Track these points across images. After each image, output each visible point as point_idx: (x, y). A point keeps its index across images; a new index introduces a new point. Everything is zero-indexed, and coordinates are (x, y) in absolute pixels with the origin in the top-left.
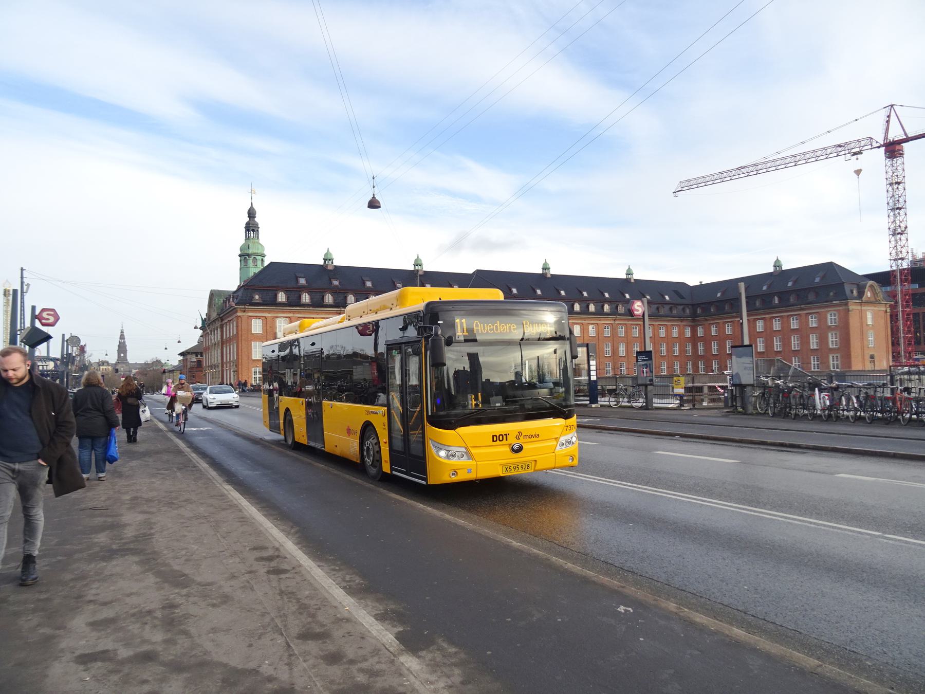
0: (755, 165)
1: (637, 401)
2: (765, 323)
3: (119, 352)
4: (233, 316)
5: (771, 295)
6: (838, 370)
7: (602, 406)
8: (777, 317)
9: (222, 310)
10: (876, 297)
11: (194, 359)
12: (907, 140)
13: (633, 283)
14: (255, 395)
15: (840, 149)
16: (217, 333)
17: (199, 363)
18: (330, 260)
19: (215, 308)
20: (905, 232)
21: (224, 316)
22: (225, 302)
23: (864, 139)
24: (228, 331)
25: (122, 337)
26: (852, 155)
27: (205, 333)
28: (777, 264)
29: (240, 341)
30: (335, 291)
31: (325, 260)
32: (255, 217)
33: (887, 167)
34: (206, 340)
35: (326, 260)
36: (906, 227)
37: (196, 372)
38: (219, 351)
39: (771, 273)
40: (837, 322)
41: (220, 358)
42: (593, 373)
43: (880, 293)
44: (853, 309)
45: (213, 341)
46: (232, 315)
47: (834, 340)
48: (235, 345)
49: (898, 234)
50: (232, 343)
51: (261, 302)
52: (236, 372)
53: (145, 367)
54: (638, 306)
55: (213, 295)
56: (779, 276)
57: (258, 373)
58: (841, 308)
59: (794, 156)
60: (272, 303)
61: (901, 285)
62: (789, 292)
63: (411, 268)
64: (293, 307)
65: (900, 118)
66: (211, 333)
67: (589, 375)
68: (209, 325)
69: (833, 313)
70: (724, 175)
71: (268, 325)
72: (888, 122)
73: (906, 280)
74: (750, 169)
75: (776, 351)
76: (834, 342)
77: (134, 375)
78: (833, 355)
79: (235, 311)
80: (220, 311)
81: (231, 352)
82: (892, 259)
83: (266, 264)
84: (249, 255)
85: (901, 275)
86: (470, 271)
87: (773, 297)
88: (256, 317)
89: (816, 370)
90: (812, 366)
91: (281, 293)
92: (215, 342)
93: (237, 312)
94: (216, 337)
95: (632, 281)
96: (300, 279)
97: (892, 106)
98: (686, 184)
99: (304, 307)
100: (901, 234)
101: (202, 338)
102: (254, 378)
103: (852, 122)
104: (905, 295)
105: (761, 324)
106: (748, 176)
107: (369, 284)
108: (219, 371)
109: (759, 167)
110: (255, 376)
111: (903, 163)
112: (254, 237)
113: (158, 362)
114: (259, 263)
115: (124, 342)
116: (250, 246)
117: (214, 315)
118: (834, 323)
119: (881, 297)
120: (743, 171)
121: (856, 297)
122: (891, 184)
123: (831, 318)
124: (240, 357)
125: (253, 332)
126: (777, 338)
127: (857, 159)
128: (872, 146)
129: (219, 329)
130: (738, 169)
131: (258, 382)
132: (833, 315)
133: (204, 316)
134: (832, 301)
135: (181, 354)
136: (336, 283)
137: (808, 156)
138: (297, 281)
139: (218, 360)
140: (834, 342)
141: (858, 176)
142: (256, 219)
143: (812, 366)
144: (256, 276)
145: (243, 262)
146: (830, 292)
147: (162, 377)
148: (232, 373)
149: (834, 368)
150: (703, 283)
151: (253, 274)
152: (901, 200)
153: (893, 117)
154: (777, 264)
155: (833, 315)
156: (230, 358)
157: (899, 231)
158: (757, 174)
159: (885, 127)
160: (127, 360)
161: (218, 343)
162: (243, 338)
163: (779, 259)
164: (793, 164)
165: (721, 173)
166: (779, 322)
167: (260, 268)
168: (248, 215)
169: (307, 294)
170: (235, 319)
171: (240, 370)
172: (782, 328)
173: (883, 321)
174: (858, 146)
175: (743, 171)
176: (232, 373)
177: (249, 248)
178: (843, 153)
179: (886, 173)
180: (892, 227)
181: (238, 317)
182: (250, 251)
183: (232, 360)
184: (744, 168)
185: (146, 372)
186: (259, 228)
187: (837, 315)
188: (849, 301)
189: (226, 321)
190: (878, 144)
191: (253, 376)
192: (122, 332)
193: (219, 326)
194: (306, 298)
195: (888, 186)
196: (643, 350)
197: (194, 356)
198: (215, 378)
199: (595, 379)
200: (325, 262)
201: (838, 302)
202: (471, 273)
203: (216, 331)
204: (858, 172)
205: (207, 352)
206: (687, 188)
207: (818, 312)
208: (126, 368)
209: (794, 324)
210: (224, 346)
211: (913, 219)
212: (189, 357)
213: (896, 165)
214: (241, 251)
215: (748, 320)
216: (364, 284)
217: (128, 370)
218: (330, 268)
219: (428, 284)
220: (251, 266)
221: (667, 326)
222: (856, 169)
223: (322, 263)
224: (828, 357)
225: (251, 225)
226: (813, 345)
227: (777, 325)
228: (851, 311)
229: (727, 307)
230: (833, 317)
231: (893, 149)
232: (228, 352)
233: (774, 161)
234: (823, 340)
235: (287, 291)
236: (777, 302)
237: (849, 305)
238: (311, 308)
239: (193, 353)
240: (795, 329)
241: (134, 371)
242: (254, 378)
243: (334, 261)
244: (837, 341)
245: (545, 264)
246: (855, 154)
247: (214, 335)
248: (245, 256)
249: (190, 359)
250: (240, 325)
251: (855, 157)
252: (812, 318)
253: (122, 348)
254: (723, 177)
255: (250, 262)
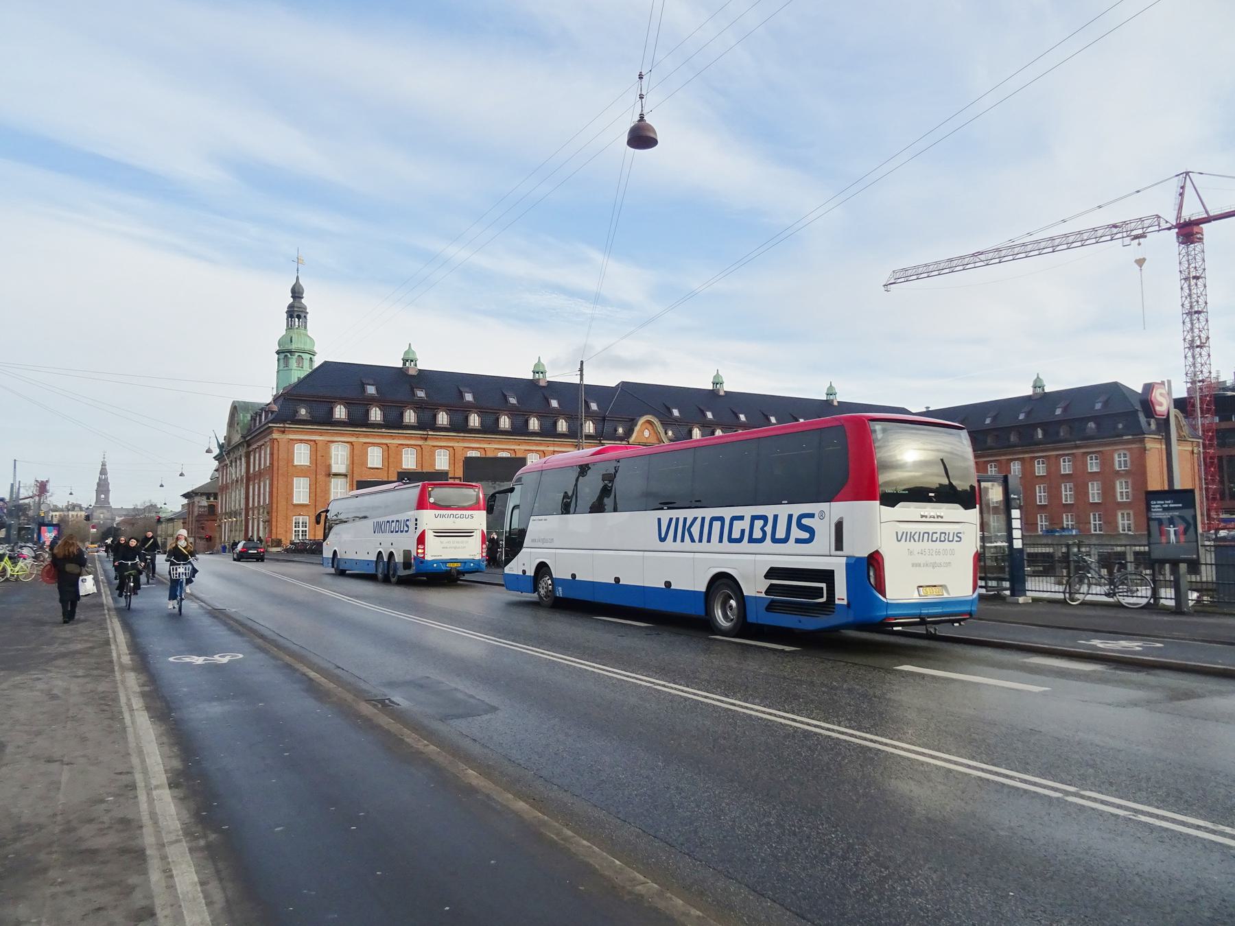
0: (998, 250)
1: (1131, 593)
2: (1023, 465)
3: (98, 492)
4: (267, 440)
5: (1034, 427)
6: (1130, 533)
7: (1035, 600)
8: (1040, 457)
9: (249, 430)
10: (1181, 432)
11: (204, 503)
12: (1208, 220)
13: (836, 406)
14: (300, 559)
15: (1115, 230)
16: (241, 465)
17: (212, 508)
18: (412, 361)
19: (239, 429)
20: (1206, 345)
21: (250, 439)
22: (253, 419)
23: (1148, 218)
24: (257, 462)
25: (103, 471)
26: (1133, 239)
27: (222, 465)
28: (1038, 384)
29: (275, 475)
30: (419, 406)
31: (405, 361)
32: (303, 298)
33: (1181, 256)
34: (223, 475)
35: (407, 361)
36: (1208, 338)
37: (206, 522)
38: (243, 491)
39: (1029, 397)
40: (1128, 465)
41: (243, 502)
42: (1017, 534)
43: (1186, 427)
44: (1151, 448)
45: (234, 476)
46: (265, 437)
47: (1124, 490)
48: (268, 482)
49: (1198, 347)
50: (262, 479)
51: (309, 419)
52: (268, 522)
53: (133, 513)
54: (1161, 394)
55: (235, 409)
56: (1040, 401)
57: (301, 525)
58: (1133, 446)
59: (1052, 239)
60: (327, 420)
61: (1201, 417)
62: (1060, 423)
63: (530, 376)
64: (357, 427)
65: (1198, 189)
66: (231, 464)
67: (1010, 539)
68: (228, 454)
69: (1122, 452)
70: (954, 263)
71: (319, 454)
72: (1181, 194)
73: (1208, 411)
74: (990, 256)
75: (1064, 504)
76: (1124, 494)
77: (117, 524)
78: (1123, 512)
79: (269, 431)
80: (245, 432)
81: (260, 494)
82: (1188, 381)
83: (316, 365)
84: (291, 352)
85: (1201, 403)
86: (613, 384)
87: (1036, 430)
88: (301, 441)
89: (1098, 532)
90: (1092, 526)
91: (339, 406)
92: (237, 478)
93: (271, 432)
94: (237, 471)
95: (836, 404)
96: (368, 387)
97: (1187, 173)
98: (901, 274)
99: (374, 428)
100: (1200, 347)
101: (216, 473)
102: (295, 531)
103: (1094, 209)
104: (1208, 431)
105: (1016, 467)
106: (987, 265)
107: (469, 397)
108: (242, 521)
109: (1003, 253)
110: (297, 529)
111: (1203, 252)
112: (299, 326)
113: (153, 507)
114: (306, 363)
115: (106, 479)
116: (293, 339)
117: (237, 438)
118: (1125, 467)
119: (1187, 432)
120: (978, 258)
121: (1153, 431)
122: (1186, 279)
123: (1120, 459)
124: (275, 500)
125: (296, 463)
126: (1040, 487)
127: (1139, 244)
128: (1159, 226)
129: (243, 459)
130: (973, 255)
131: (300, 537)
132: (1122, 455)
133: (222, 441)
134: (1122, 436)
135: (185, 496)
136: (421, 394)
137: (1071, 239)
138: (364, 390)
139: (240, 505)
140: (1124, 494)
141: (1141, 267)
142: (303, 301)
143: (1092, 526)
144: (301, 382)
145: (282, 361)
146: (1119, 423)
147: (157, 528)
148: (261, 524)
149: (1096, 531)
150: (930, 409)
151: (296, 380)
152: (1201, 301)
153: (1189, 190)
154: (1038, 384)
155: (1122, 455)
156: (259, 502)
157: (1198, 343)
158: (1000, 262)
159: (1178, 201)
160: (109, 503)
161: (242, 480)
162: (280, 472)
163: (1040, 377)
164: (1051, 250)
165: (951, 260)
166: (995, 467)
167: (307, 370)
168: (291, 295)
169: (377, 409)
170: (268, 443)
171: (274, 520)
172: (1049, 472)
173: (1189, 466)
174: (1140, 227)
175: (978, 258)
176: (261, 524)
177: (291, 342)
178: (1119, 235)
179: (1180, 263)
180: (1189, 337)
181: (273, 440)
182: (293, 347)
183: (262, 504)
184: (982, 253)
185: (134, 521)
186: (307, 313)
187: (1128, 455)
188: (1146, 436)
189: (255, 446)
190: (1168, 224)
191: (294, 529)
192: (104, 465)
193: (243, 454)
194: (376, 415)
195: (1183, 281)
196: (1166, 488)
197: (204, 498)
198: (236, 530)
199: (1020, 546)
200: (405, 364)
201: (1130, 437)
202: (614, 386)
203: (238, 462)
204: (1140, 262)
205: (224, 492)
206: (902, 280)
207: (1100, 451)
208: (108, 515)
209: (1066, 468)
210: (251, 483)
211: (1216, 328)
212: (197, 499)
213: (1193, 253)
214: (279, 345)
215: (976, 462)
216: (461, 396)
217: (110, 517)
218: (412, 372)
219: (555, 399)
220: (294, 368)
221: (1103, 453)
222: (1138, 258)
223: (400, 365)
224: (1116, 515)
225: (295, 309)
226: (1093, 497)
227: (1040, 469)
228: (1149, 450)
229: (1013, 438)
230: (1122, 459)
231: (1188, 232)
232: (256, 493)
233: (1024, 245)
234: (1108, 491)
235: (348, 404)
236: (1040, 436)
237: (1146, 442)
238: (383, 430)
239: (202, 494)
240: (1042, 476)
241: (118, 519)
242: (295, 531)
243: (418, 362)
244: (1128, 492)
245: (717, 376)
246: (1136, 237)
247: (236, 467)
248: (285, 353)
249: (199, 502)
250: (275, 452)
251: (1137, 241)
252: (1092, 460)
253: (103, 487)
254: (951, 266)
255: (293, 362)
